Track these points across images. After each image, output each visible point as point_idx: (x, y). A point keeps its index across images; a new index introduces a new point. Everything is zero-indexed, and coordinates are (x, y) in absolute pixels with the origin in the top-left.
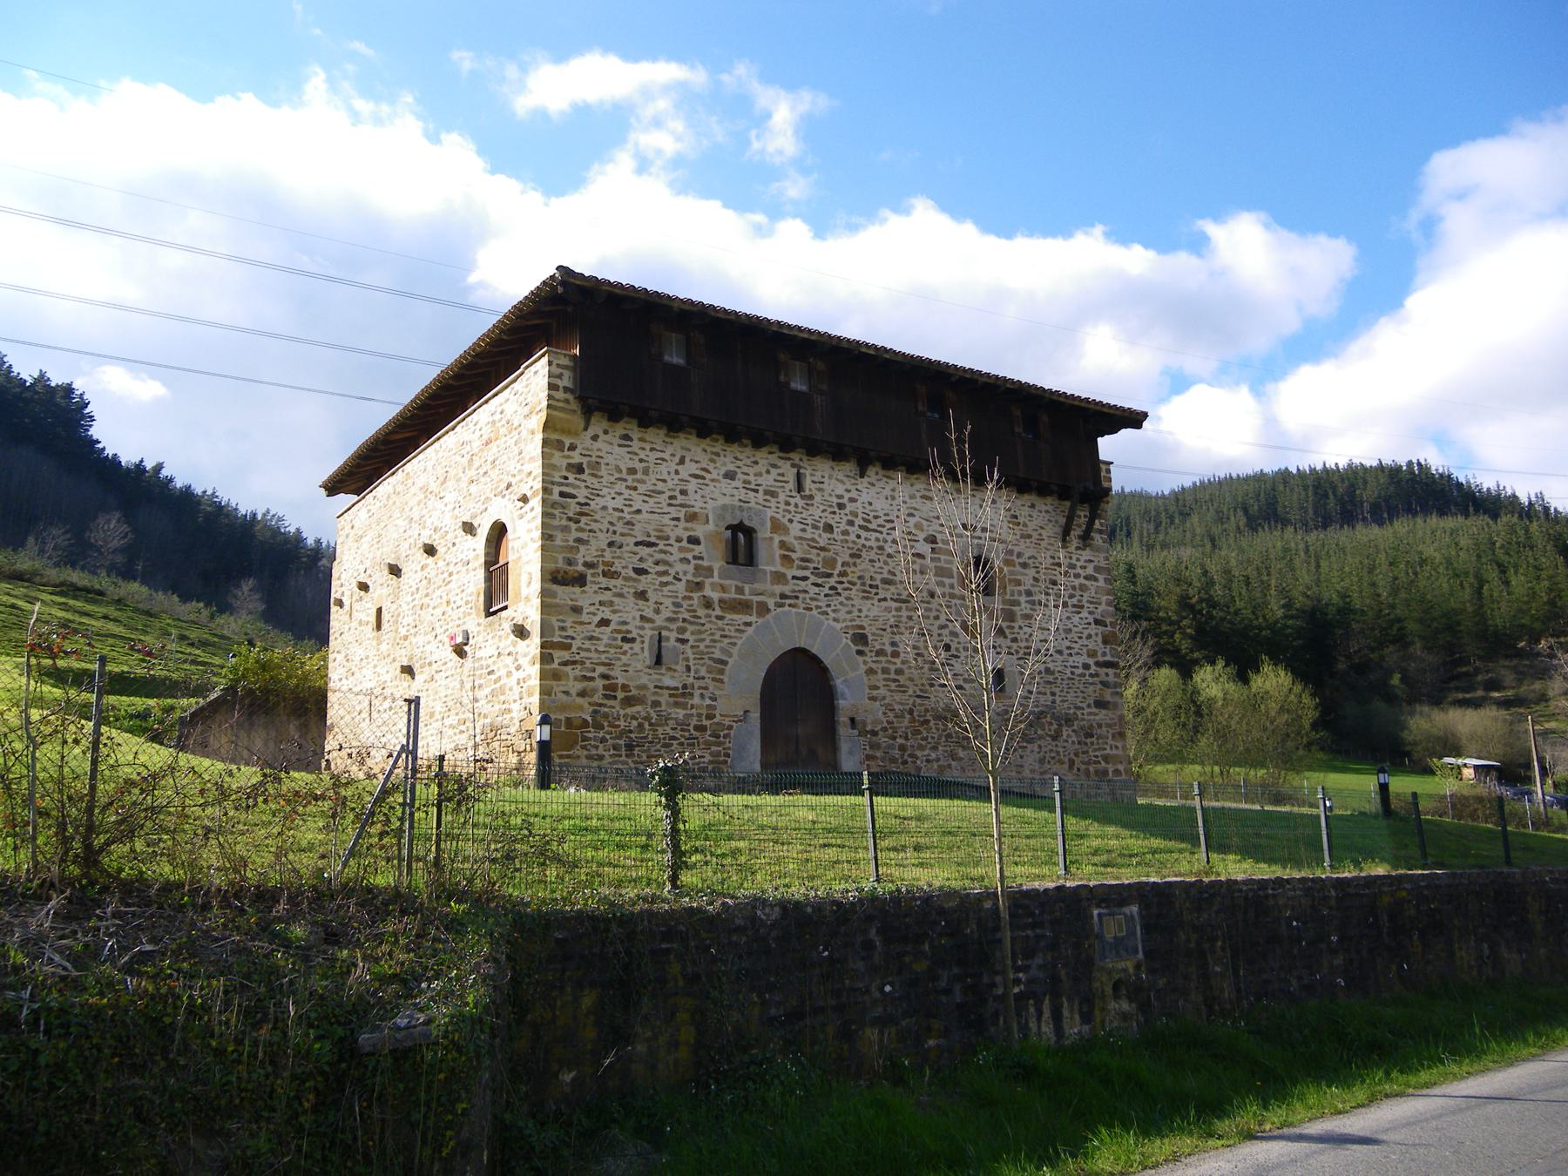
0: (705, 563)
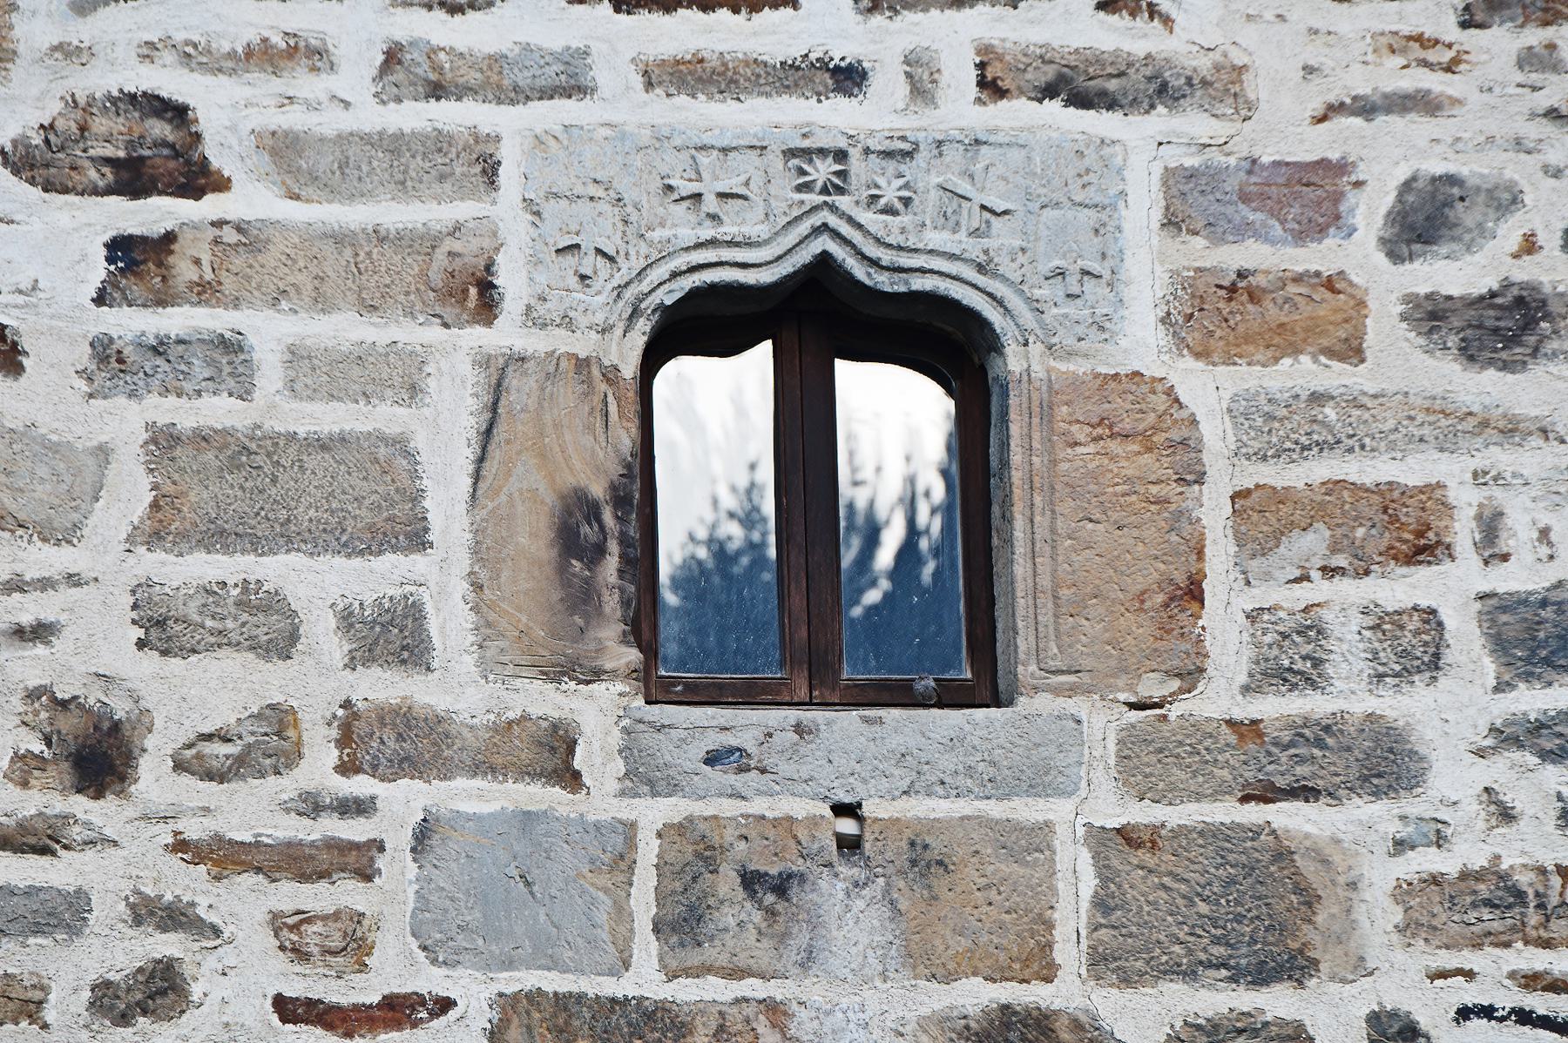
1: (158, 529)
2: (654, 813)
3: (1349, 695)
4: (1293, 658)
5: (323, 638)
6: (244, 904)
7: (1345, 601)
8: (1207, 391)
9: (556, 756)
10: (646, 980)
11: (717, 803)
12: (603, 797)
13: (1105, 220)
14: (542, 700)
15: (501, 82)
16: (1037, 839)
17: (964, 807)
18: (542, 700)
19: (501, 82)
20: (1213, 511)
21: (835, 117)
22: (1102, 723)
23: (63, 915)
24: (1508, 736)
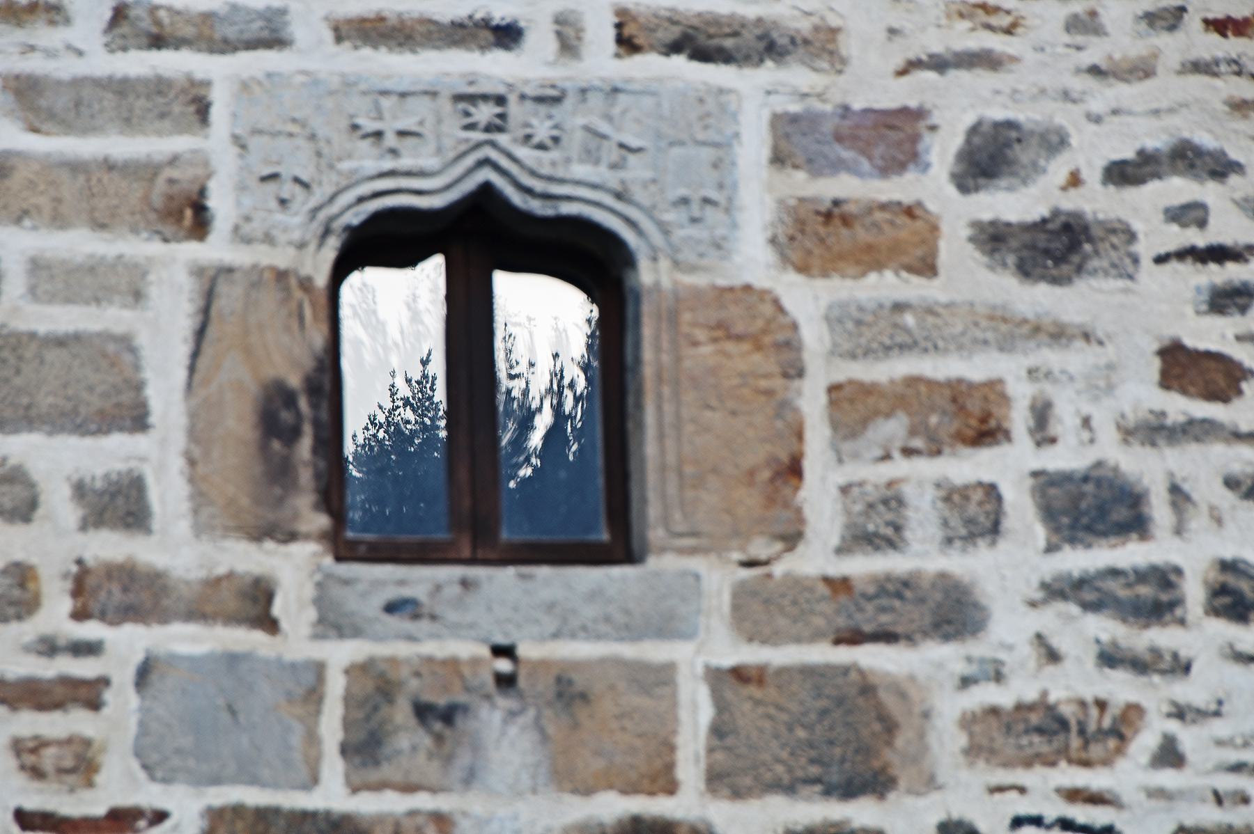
2: (341, 654)
3: (923, 555)
4: (877, 525)
5: (60, 506)
7: (922, 476)
8: (807, 301)
9: (256, 603)
10: (331, 794)
11: (398, 646)
12: (297, 639)
13: (722, 154)
14: (245, 558)
18: (245, 558)
20: (811, 402)
22: (718, 578)
24: (1059, 590)
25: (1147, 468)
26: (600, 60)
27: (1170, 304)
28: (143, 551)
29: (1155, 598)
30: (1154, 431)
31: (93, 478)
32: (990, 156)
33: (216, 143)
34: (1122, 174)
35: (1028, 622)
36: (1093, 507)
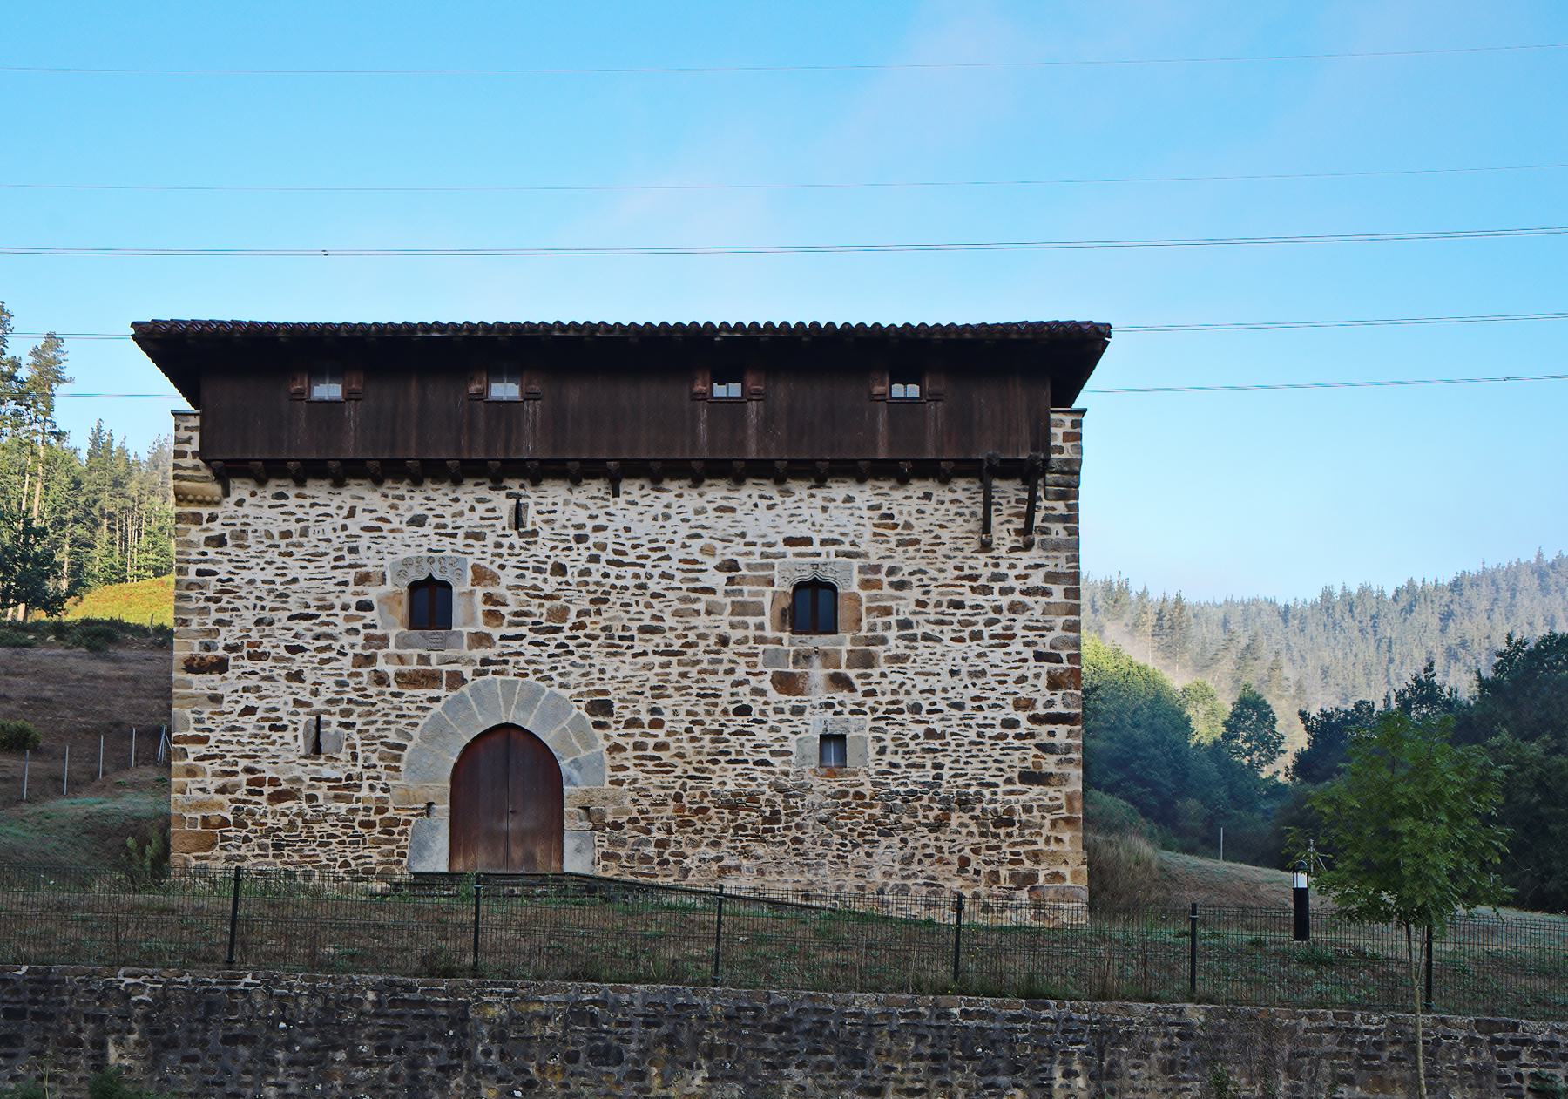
0: (378, 632)
1: (732, 614)
2: (792, 649)
3: (879, 632)
4: (873, 628)
5: (752, 627)
6: (742, 660)
7: (879, 620)
8: (863, 594)
9: (780, 641)
10: (791, 669)
11: (800, 647)
12: (786, 647)
13: (851, 572)
14: (779, 635)
15: (775, 556)
16: (839, 652)
17: (1421, 1064)
18: (779, 635)
19: (775, 556)
20: (863, 610)
21: (817, 560)
22: (848, 636)
23: (720, 662)
24: (900, 637)
25: (913, 618)
26: (833, 558)
27: (916, 593)
28: (764, 634)
29: (913, 638)
30: (914, 613)
31: (1252, 712)
32: (892, 571)
33: (776, 572)
34: (911, 574)
35: (895, 644)
36: (905, 624)
